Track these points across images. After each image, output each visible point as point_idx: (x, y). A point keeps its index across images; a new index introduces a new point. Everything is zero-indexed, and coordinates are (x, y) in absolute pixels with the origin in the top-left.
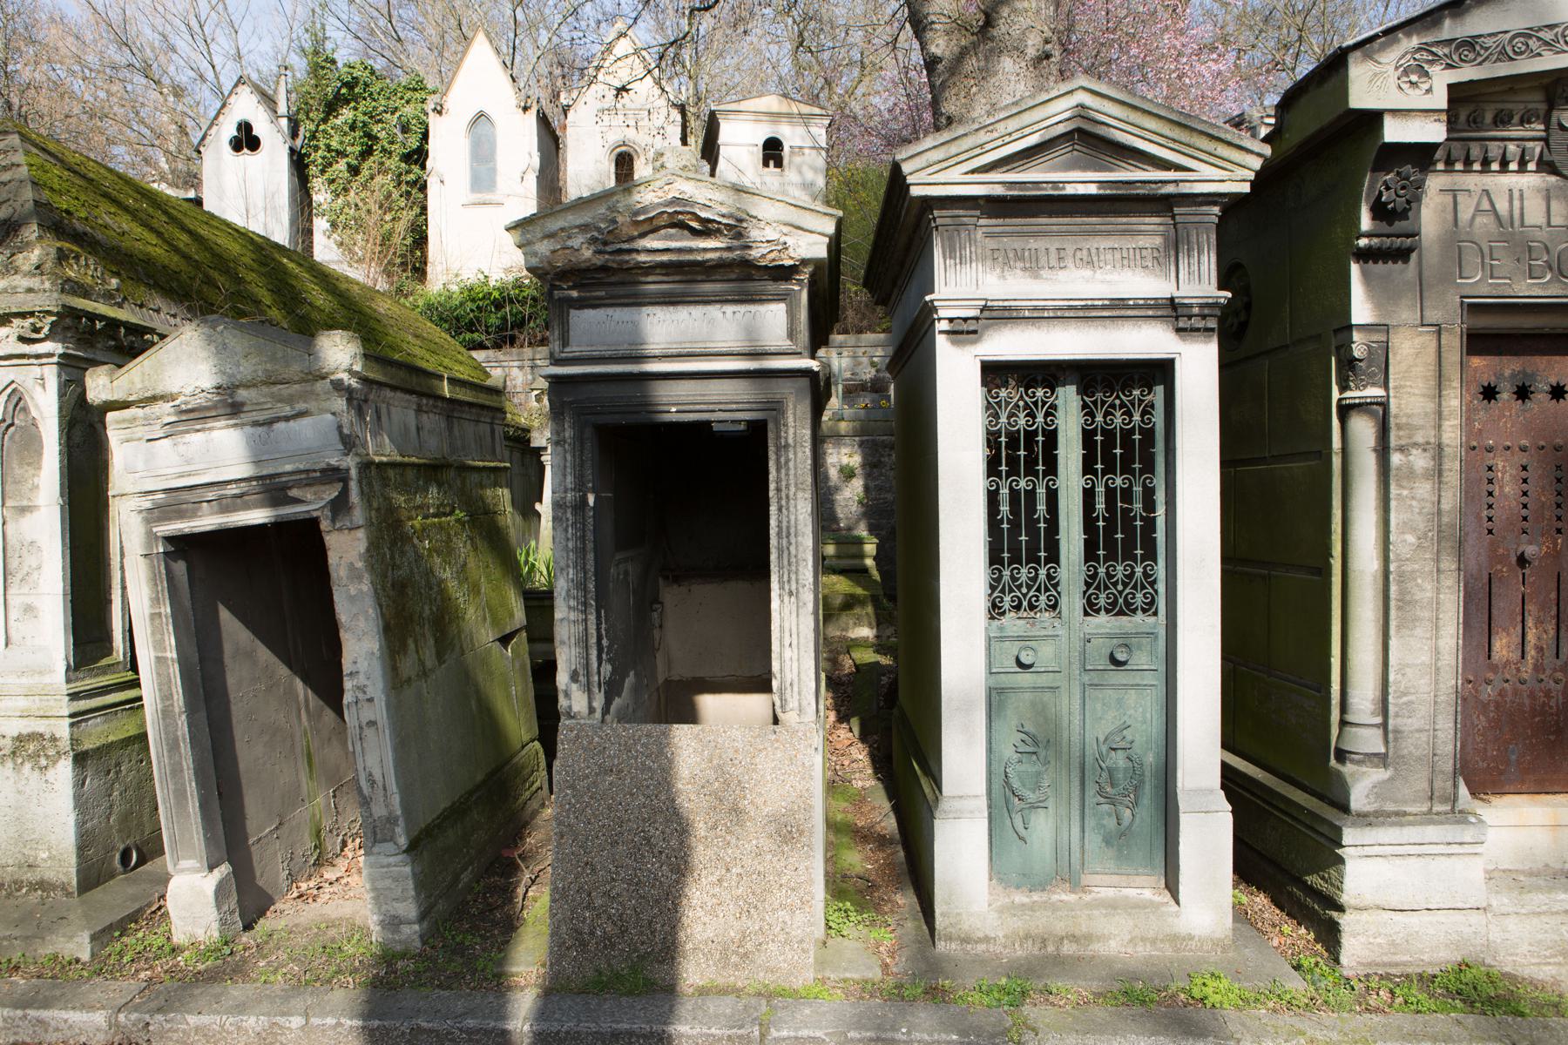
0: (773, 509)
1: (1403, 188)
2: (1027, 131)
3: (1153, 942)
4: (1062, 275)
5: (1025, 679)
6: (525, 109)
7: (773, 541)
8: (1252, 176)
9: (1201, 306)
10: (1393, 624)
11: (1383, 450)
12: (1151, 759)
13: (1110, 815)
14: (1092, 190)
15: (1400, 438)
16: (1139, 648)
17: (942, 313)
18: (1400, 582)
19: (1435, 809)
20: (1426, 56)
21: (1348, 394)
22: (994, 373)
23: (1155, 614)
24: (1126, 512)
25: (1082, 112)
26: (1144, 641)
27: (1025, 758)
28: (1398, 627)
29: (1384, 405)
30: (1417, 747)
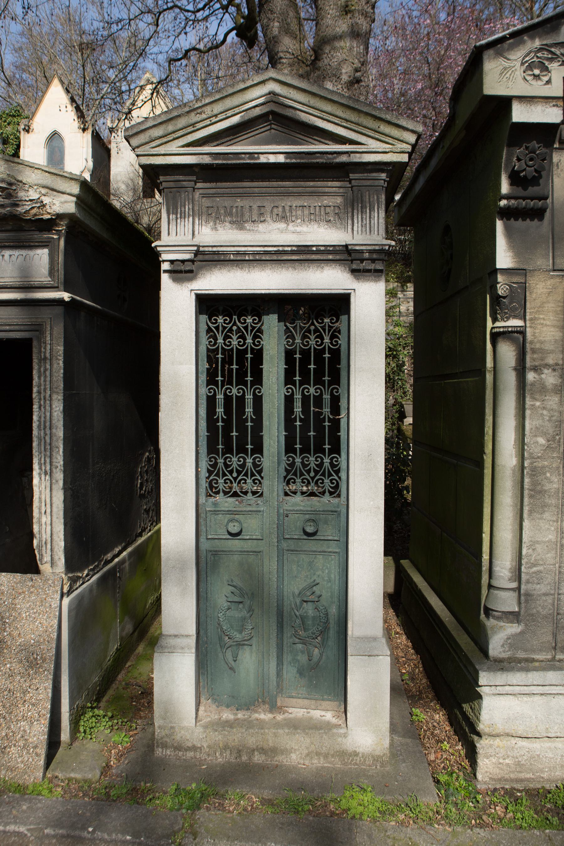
0: (35, 407)
1: (531, 159)
2: (230, 113)
3: (326, 756)
4: (261, 227)
5: (235, 544)
6: (84, 130)
7: (35, 432)
8: (409, 148)
9: (370, 252)
10: (526, 509)
11: (521, 370)
12: (333, 610)
13: (303, 652)
14: (281, 159)
15: (534, 360)
16: (326, 522)
17: (164, 257)
18: (532, 476)
19: (558, 657)
20: (546, 55)
21: (498, 324)
22: (207, 304)
23: (339, 496)
24: (318, 415)
25: (273, 97)
26: (330, 517)
27: (233, 606)
28: (531, 512)
29: (522, 332)
30: (543, 608)
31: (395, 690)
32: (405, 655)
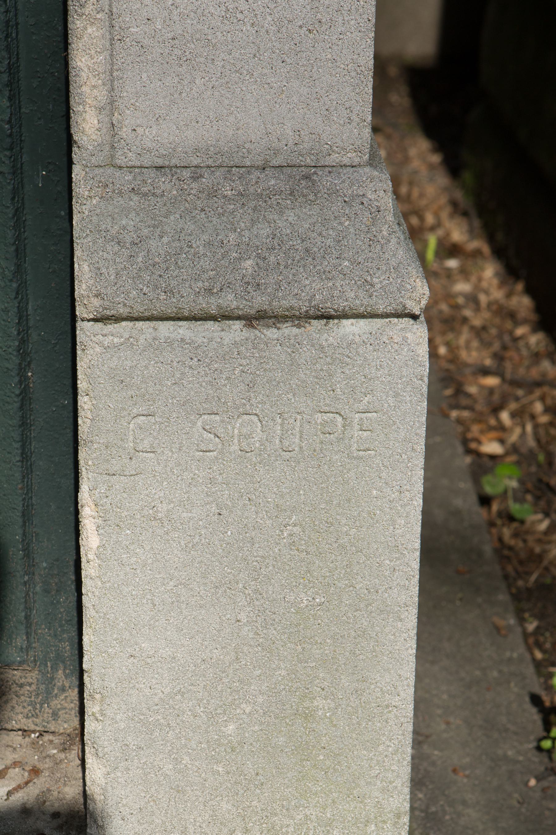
31: (446, 557)
32: (499, 357)
